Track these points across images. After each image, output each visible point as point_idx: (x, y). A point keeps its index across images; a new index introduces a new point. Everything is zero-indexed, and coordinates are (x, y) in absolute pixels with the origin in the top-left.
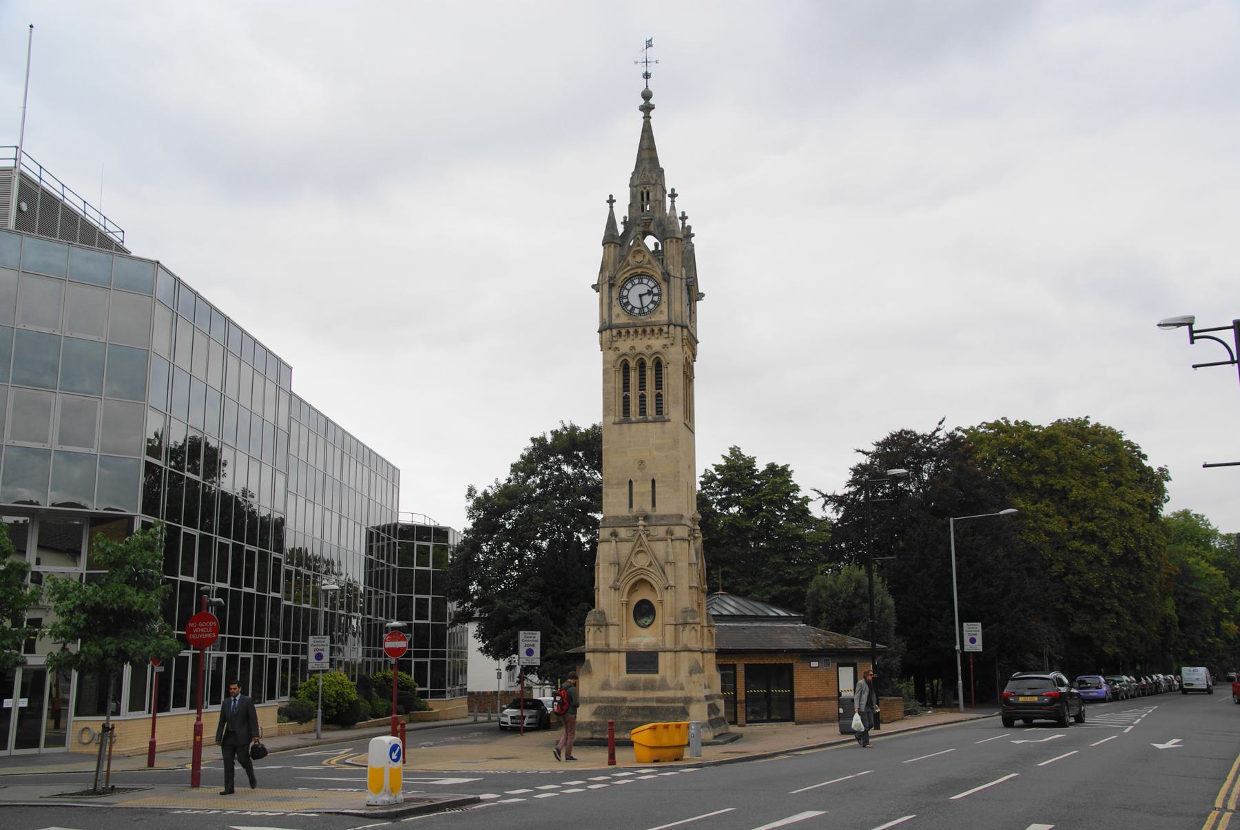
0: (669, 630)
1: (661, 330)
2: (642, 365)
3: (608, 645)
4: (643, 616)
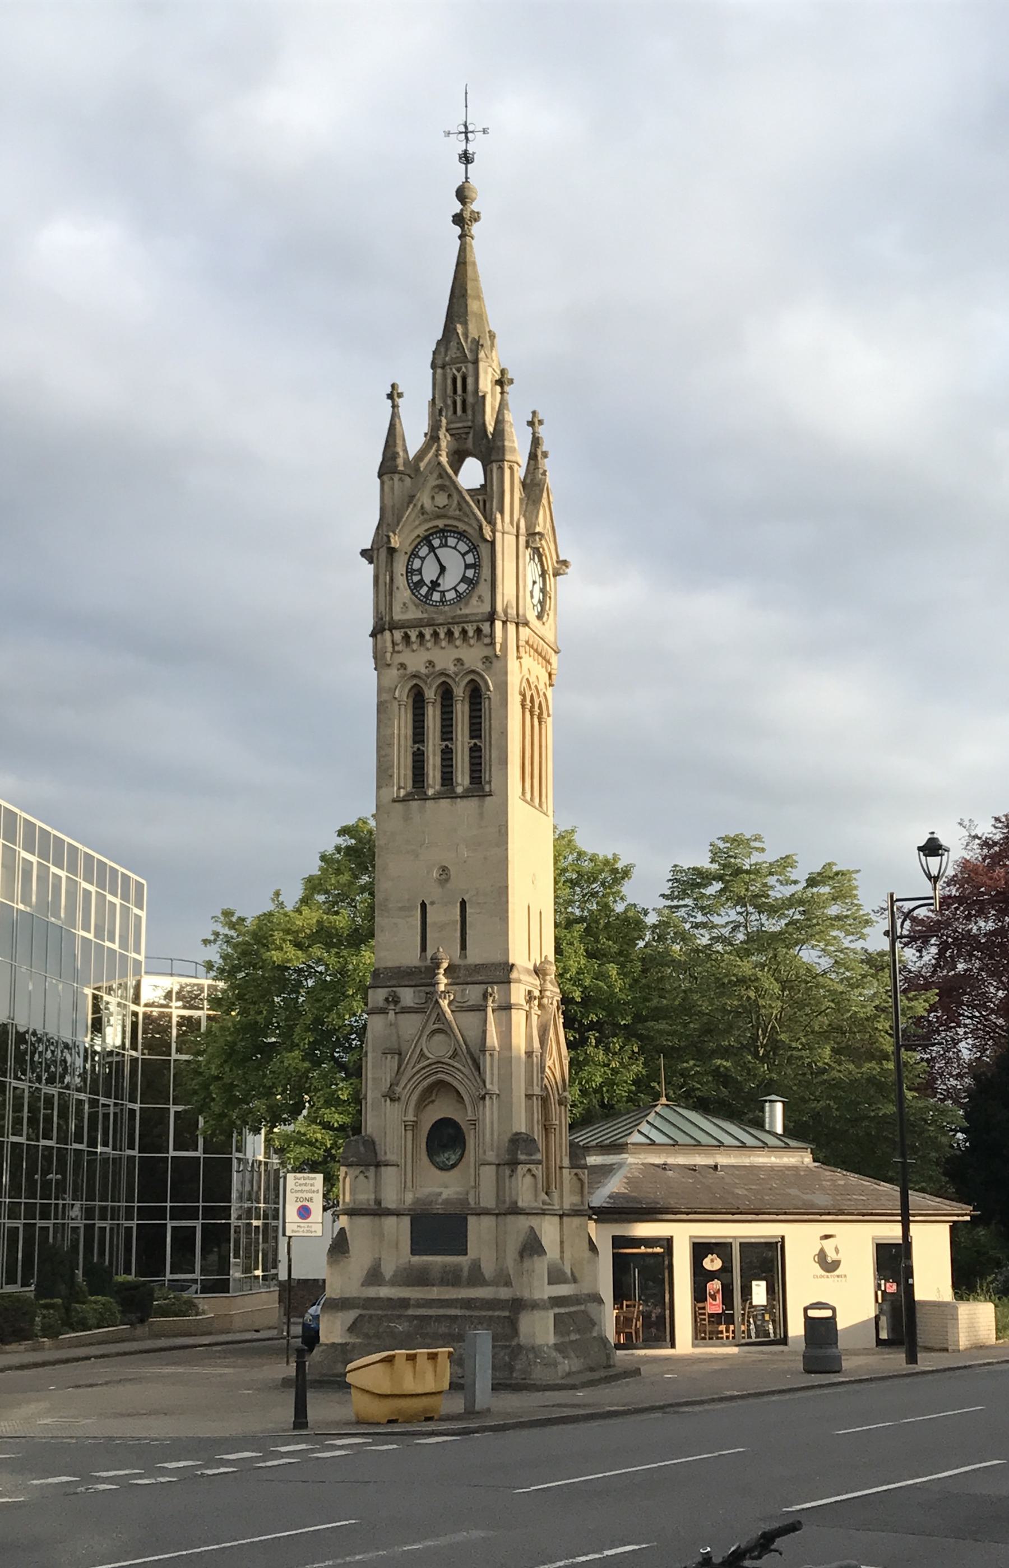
0: (488, 1173)
1: (479, 631)
2: (447, 695)
3: (378, 1202)
4: (445, 1147)
